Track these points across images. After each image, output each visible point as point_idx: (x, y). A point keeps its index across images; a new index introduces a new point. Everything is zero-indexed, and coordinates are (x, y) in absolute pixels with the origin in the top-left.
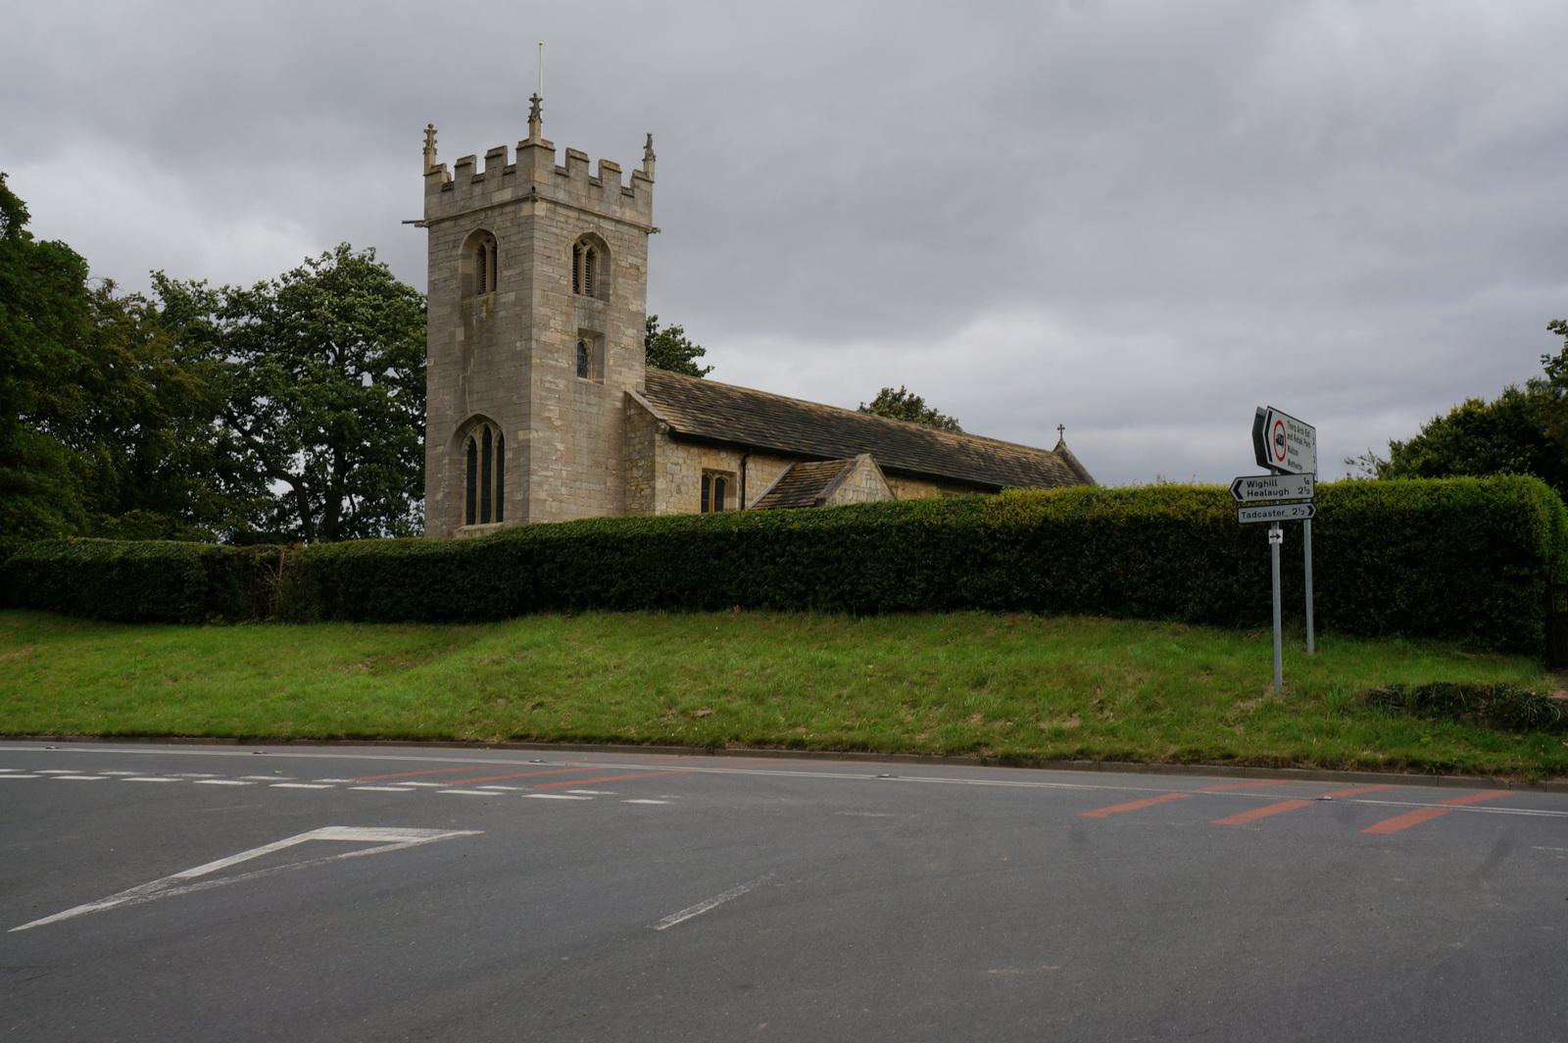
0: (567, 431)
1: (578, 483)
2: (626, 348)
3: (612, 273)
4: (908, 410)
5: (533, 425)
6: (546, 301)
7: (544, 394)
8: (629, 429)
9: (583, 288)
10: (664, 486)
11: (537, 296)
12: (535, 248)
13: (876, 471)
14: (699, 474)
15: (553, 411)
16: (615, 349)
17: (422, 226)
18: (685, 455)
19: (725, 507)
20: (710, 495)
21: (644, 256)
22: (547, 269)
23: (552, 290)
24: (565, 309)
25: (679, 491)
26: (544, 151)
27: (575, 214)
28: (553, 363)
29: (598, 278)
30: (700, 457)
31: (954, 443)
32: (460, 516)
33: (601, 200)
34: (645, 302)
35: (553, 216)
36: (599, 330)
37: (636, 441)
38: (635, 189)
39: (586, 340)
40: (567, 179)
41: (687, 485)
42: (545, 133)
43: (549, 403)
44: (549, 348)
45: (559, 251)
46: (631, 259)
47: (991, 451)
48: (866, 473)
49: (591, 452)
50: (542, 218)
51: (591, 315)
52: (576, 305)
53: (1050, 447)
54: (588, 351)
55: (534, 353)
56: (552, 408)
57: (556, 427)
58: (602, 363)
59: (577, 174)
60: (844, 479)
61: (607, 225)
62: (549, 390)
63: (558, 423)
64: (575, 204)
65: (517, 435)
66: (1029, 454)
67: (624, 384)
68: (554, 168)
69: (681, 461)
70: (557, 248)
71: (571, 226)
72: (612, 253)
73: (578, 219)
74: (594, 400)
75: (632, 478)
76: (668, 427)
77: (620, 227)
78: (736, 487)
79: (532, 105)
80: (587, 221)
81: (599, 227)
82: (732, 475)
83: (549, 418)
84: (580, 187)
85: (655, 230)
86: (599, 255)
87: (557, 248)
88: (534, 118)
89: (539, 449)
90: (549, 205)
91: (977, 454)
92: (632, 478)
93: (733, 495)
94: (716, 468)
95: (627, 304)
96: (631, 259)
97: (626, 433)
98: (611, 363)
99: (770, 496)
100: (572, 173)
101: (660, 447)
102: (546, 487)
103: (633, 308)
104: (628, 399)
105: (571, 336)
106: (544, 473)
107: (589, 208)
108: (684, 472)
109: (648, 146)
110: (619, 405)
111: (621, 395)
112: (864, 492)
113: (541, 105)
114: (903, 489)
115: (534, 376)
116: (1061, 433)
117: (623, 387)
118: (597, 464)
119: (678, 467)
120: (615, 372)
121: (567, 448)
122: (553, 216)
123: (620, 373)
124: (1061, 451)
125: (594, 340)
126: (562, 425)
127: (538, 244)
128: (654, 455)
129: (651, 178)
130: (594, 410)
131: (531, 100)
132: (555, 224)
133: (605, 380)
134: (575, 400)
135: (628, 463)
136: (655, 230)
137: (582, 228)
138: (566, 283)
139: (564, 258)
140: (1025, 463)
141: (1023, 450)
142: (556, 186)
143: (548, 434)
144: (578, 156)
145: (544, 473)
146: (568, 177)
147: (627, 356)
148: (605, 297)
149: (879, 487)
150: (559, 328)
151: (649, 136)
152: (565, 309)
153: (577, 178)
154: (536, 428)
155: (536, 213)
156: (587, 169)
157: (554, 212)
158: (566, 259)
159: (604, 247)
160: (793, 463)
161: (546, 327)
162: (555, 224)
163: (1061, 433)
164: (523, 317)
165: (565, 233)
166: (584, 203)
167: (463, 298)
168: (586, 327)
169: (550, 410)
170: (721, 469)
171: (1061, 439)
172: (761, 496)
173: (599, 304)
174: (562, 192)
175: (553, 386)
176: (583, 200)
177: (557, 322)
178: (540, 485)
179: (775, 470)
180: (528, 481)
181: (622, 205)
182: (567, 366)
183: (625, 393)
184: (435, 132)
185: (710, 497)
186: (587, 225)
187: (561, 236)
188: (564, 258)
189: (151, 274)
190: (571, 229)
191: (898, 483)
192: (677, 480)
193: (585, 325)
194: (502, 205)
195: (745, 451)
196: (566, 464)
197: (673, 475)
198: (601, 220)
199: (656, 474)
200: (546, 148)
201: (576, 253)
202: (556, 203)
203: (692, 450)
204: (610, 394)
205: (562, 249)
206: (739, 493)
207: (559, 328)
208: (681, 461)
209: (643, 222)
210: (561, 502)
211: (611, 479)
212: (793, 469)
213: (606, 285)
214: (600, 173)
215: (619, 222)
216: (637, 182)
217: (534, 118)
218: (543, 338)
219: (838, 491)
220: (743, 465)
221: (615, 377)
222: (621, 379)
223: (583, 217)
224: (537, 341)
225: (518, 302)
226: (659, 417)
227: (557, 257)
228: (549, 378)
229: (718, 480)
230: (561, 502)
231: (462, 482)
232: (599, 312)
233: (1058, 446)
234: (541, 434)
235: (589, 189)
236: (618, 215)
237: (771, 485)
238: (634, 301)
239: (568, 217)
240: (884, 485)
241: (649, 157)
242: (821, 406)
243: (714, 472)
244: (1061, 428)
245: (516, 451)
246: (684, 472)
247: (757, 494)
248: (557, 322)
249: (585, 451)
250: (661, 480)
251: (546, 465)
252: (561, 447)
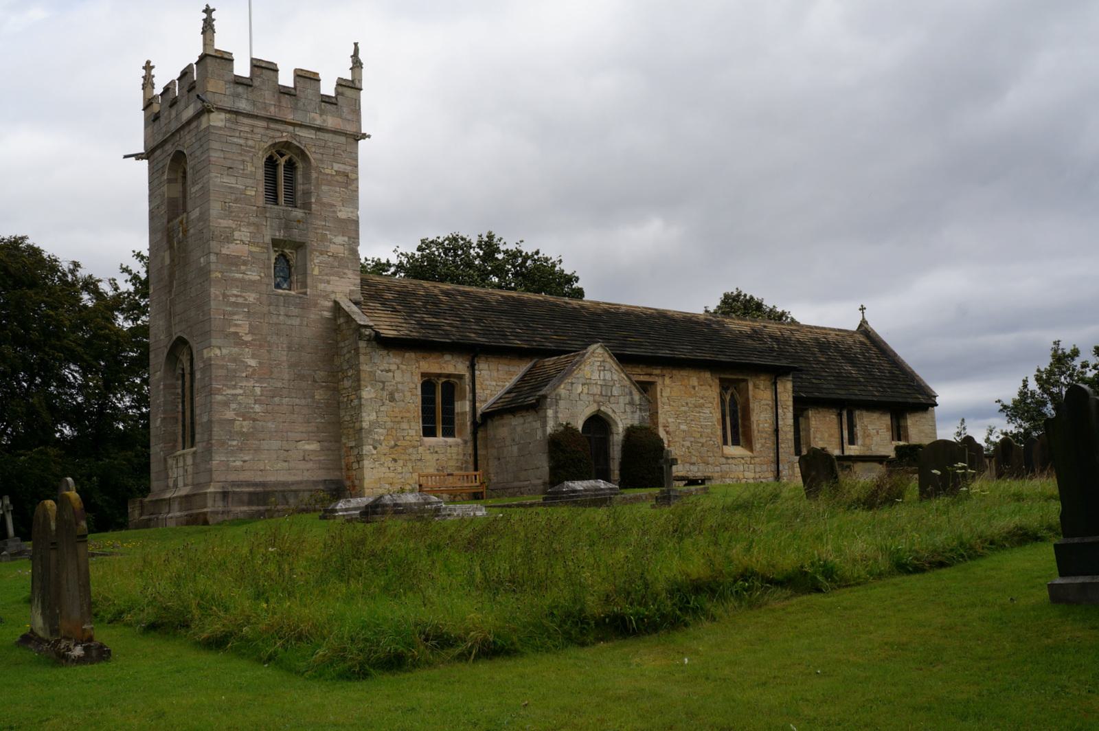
0: (261, 346)
1: (277, 399)
2: (334, 257)
3: (313, 182)
4: (745, 308)
5: (214, 342)
6: (228, 212)
7: (229, 309)
8: (339, 339)
9: (282, 199)
10: (373, 395)
11: (215, 208)
12: (212, 159)
13: (609, 360)
14: (418, 381)
15: (242, 325)
16: (321, 258)
17: (142, 159)
18: (398, 361)
19: (456, 411)
20: (437, 399)
21: (354, 163)
22: (229, 181)
23: (236, 201)
25: (392, 399)
26: (218, 60)
27: (264, 124)
29: (300, 188)
30: (418, 362)
31: (747, 329)
32: (176, 441)
33: (295, 109)
34: (358, 209)
36: (298, 239)
37: (345, 350)
39: (287, 251)
40: (250, 89)
41: (403, 392)
42: (220, 44)
44: (233, 261)
45: (243, 161)
46: (336, 167)
47: (787, 334)
48: (599, 364)
49: (292, 366)
50: (220, 128)
51: (287, 225)
52: (268, 215)
53: (853, 326)
54: (291, 262)
55: (213, 267)
57: (246, 343)
58: (305, 274)
59: (263, 82)
60: (571, 372)
61: (303, 133)
62: (236, 304)
63: (248, 338)
64: (262, 113)
65: (202, 354)
66: (829, 334)
67: (333, 292)
68: (233, 77)
69: (393, 367)
70: (240, 158)
72: (313, 161)
73: (268, 128)
74: (294, 311)
75: (344, 389)
76: (373, 333)
77: (321, 135)
78: (465, 390)
79: (205, 16)
80: (278, 130)
81: (295, 136)
82: (461, 377)
83: (236, 334)
84: (268, 97)
85: (364, 136)
86: (300, 165)
87: (240, 158)
88: (208, 27)
89: (222, 367)
90: (228, 116)
91: (771, 337)
92: (344, 389)
93: (463, 398)
94: (438, 371)
95: (335, 212)
96: (336, 167)
97: (337, 343)
98: (316, 272)
99: (507, 396)
101: (365, 354)
102: (233, 406)
103: (342, 215)
104: (337, 307)
106: (229, 392)
107: (280, 116)
108: (398, 379)
109: (355, 56)
110: (327, 314)
111: (330, 304)
112: (596, 384)
113: (214, 15)
116: (863, 313)
117: (333, 296)
118: (301, 377)
119: (390, 374)
120: (322, 281)
121: (260, 363)
123: (328, 282)
124: (864, 329)
125: (296, 251)
127: (215, 155)
129: (357, 85)
130: (296, 322)
131: (204, 11)
133: (309, 291)
134: (270, 313)
135: (340, 374)
136: (364, 136)
137: (273, 138)
138: (253, 193)
140: (824, 343)
141: (824, 331)
142: (238, 96)
143: (236, 350)
144: (264, 65)
145: (229, 392)
146: (251, 86)
147: (336, 264)
148: (307, 206)
149: (615, 377)
150: (246, 240)
151: (356, 44)
153: (263, 87)
154: (218, 344)
155: (211, 124)
156: (277, 78)
158: (253, 169)
159: (302, 154)
160: (535, 360)
161: (229, 239)
162: (237, 135)
163: (863, 313)
164: (204, 231)
165: (250, 143)
167: (168, 222)
169: (236, 325)
170: (446, 372)
171: (863, 319)
172: (497, 396)
173: (298, 213)
174: (244, 101)
175: (240, 300)
176: (272, 109)
180: (211, 402)
181: (322, 112)
182: (259, 278)
183: (336, 302)
184: (153, 67)
185: (437, 402)
186: (279, 134)
187: (247, 146)
189: (133, 254)
190: (260, 139)
191: (665, 372)
193: (280, 235)
194: (189, 122)
195: (473, 352)
196: (260, 380)
198: (297, 129)
200: (222, 58)
202: (237, 113)
203: (407, 355)
204: (316, 305)
205: (248, 159)
206: (469, 396)
207: (246, 240)
208: (393, 367)
209: (350, 128)
210: (254, 420)
211: (321, 391)
212: (534, 366)
213: (307, 193)
214: (337, 93)
215: (319, 129)
216: (341, 89)
217: (208, 27)
218: (224, 251)
219: (562, 386)
220: (472, 367)
221: (321, 286)
222: (329, 288)
223: (272, 126)
225: (200, 219)
226: (362, 323)
227: (242, 167)
230: (254, 420)
231: (177, 407)
232: (299, 221)
233: (861, 325)
234: (225, 351)
235: (279, 98)
236: (319, 123)
237: (508, 385)
238: (343, 208)
240: (623, 375)
241: (357, 64)
242: (598, 303)
243: (439, 376)
244: (862, 309)
245: (204, 370)
246: (398, 379)
248: (243, 234)
249: (285, 365)
250: (369, 388)
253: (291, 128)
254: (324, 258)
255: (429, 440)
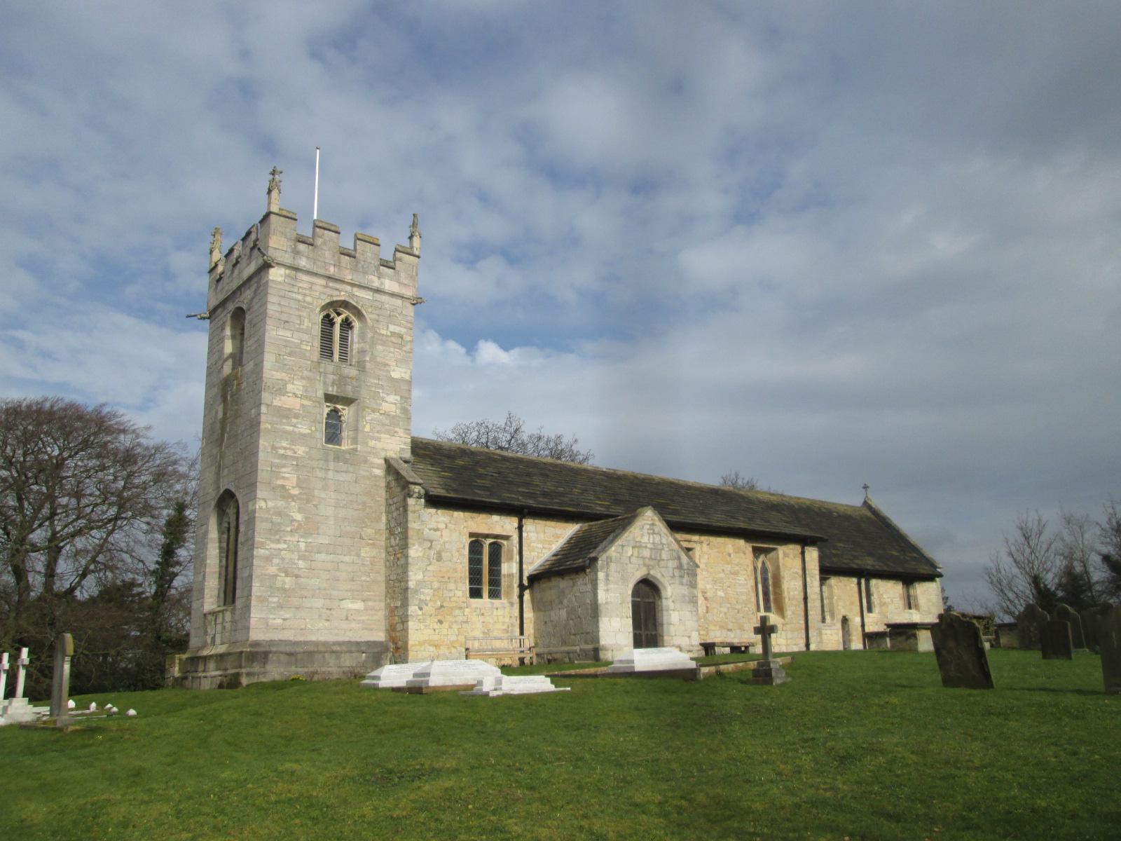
14: (467, 541)
23: (290, 354)
24: (306, 373)
27: (322, 282)
28: (291, 428)
33: (355, 269)
35: (293, 282)
38: (397, 262)
43: (283, 470)
44: (285, 414)
46: (392, 328)
48: (648, 527)
55: (263, 418)
56: (287, 475)
57: (292, 497)
59: (324, 243)
62: (284, 457)
63: (295, 492)
69: (442, 526)
70: (297, 313)
71: (317, 294)
72: (369, 321)
73: (327, 286)
77: (377, 296)
80: (337, 290)
82: (507, 538)
83: (283, 487)
86: (356, 324)
87: (297, 313)
89: (266, 520)
90: (288, 271)
93: (510, 559)
96: (392, 328)
98: (367, 429)
100: (319, 242)
102: (276, 561)
105: (314, 402)
112: (646, 547)
114: (708, 545)
115: (263, 443)
119: (438, 533)
122: (293, 282)
124: (866, 504)
126: (301, 494)
128: (407, 522)
132: (296, 290)
137: (331, 296)
139: (307, 323)
143: (281, 503)
149: (664, 541)
152: (306, 373)
153: (324, 247)
157: (296, 279)
161: (281, 391)
165: (308, 299)
166: (332, 270)
168: (334, 393)
175: (289, 453)
177: (297, 386)
178: (268, 559)
179: (559, 532)
186: (338, 293)
188: (307, 323)
190: (317, 294)
192: (437, 546)
197: (431, 541)
199: (410, 541)
201: (328, 322)
202: (297, 269)
206: (517, 558)
210: (297, 576)
215: (378, 291)
216: (399, 255)
218: (277, 403)
219: (613, 548)
221: (372, 443)
222: (379, 445)
223: (331, 284)
224: (268, 406)
228: (284, 444)
229: (491, 544)
230: (297, 576)
236: (376, 284)
239: (312, 283)
240: (671, 539)
244: (866, 487)
247: (538, 558)
248: (297, 386)
250: (416, 547)
251: (277, 537)
252: (298, 517)
253: (349, 288)
254: (376, 416)
255: (476, 602)
